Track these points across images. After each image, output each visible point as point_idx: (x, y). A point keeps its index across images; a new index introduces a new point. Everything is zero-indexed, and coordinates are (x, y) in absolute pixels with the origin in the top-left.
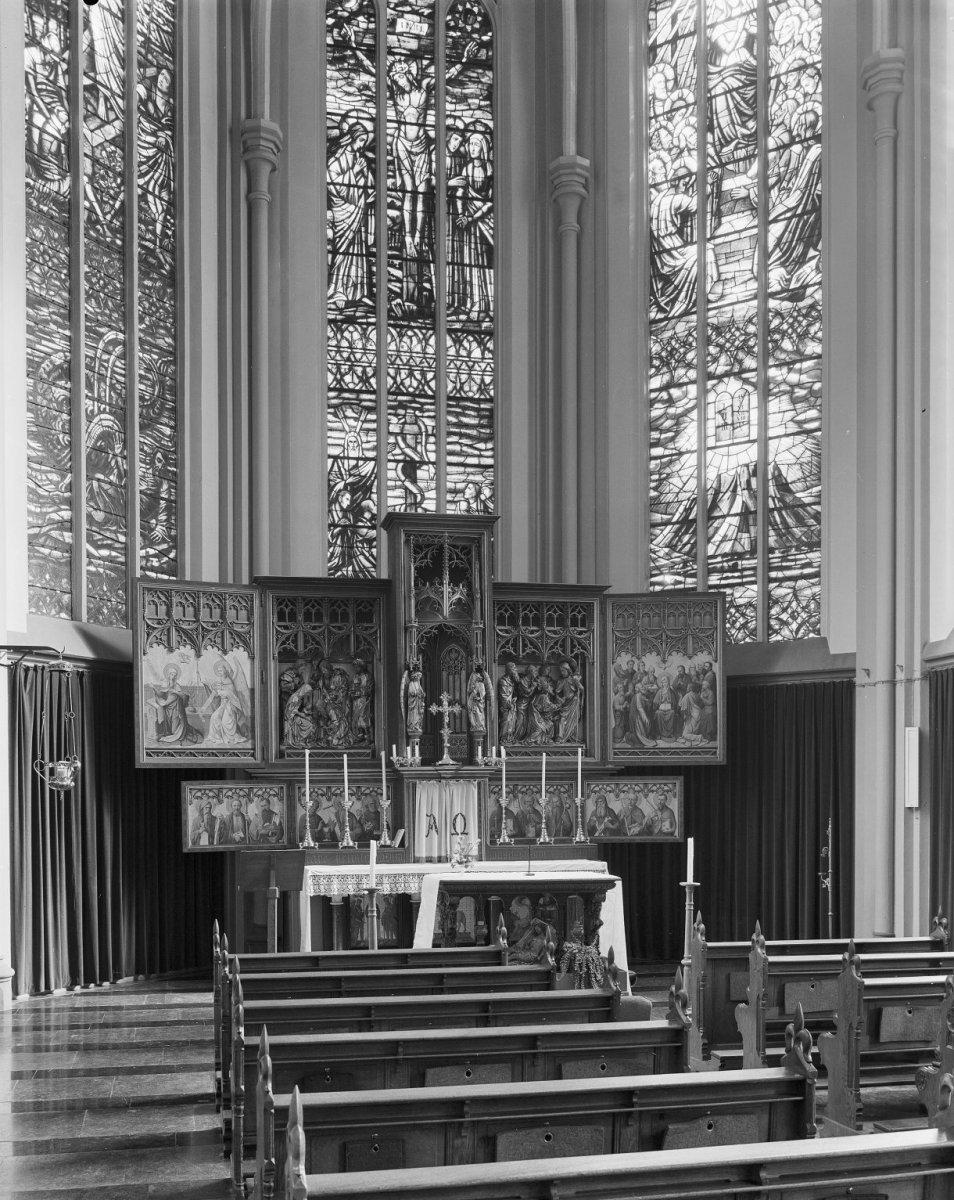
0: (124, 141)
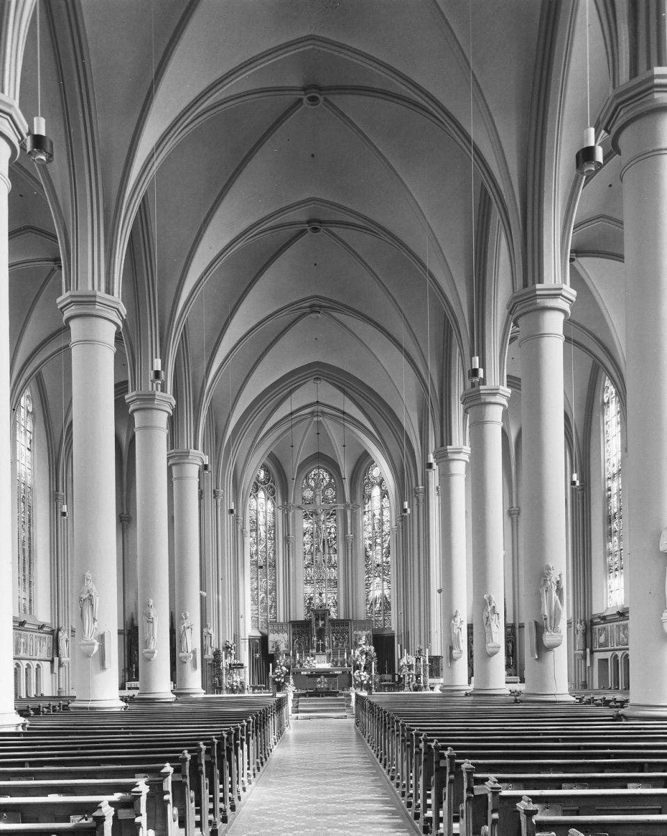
0: (266, 546)
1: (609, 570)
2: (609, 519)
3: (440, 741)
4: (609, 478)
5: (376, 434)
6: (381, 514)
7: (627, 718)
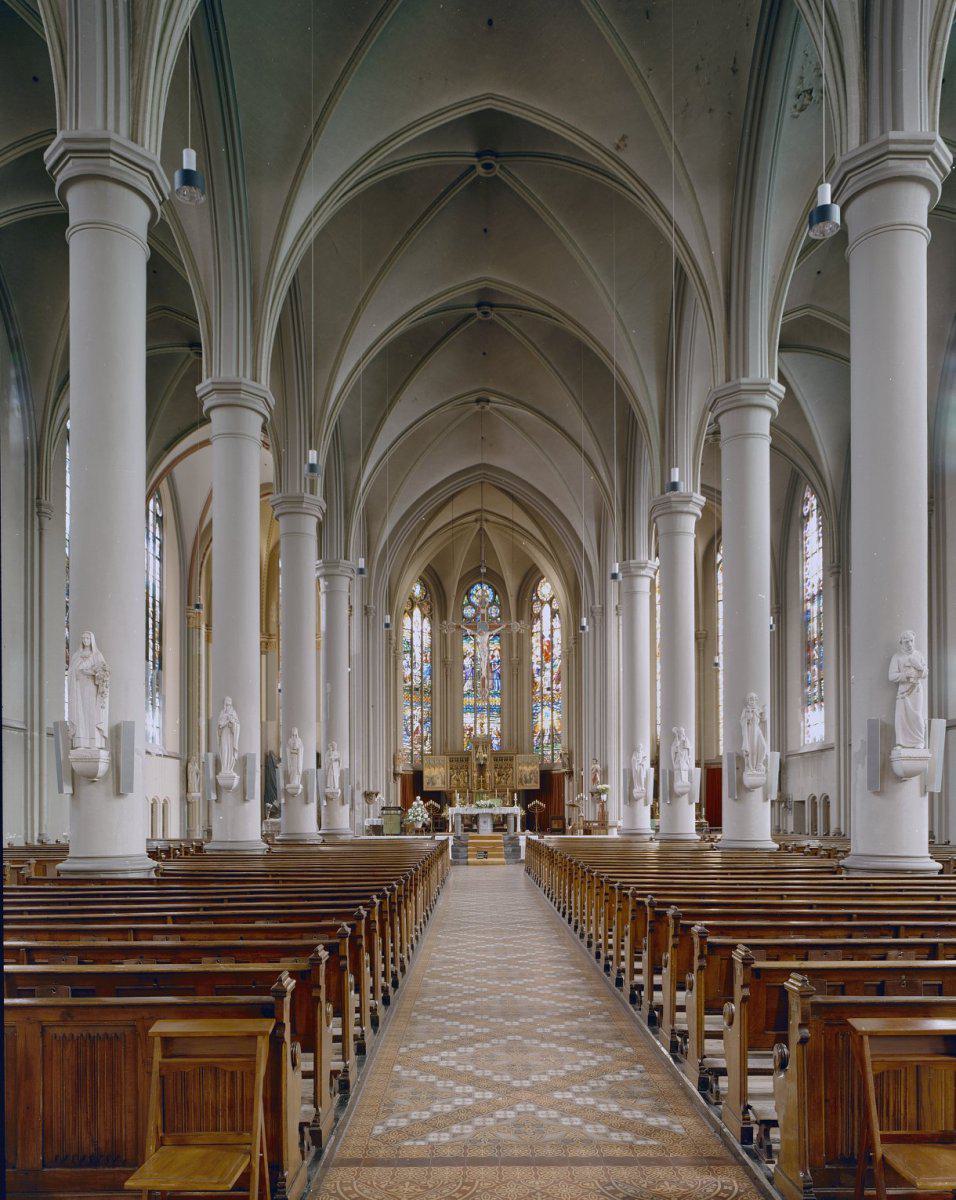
0: (422, 669)
1: (808, 702)
2: (808, 646)
3: (655, 895)
4: (807, 600)
5: (545, 544)
6: (551, 636)
7: (848, 869)
